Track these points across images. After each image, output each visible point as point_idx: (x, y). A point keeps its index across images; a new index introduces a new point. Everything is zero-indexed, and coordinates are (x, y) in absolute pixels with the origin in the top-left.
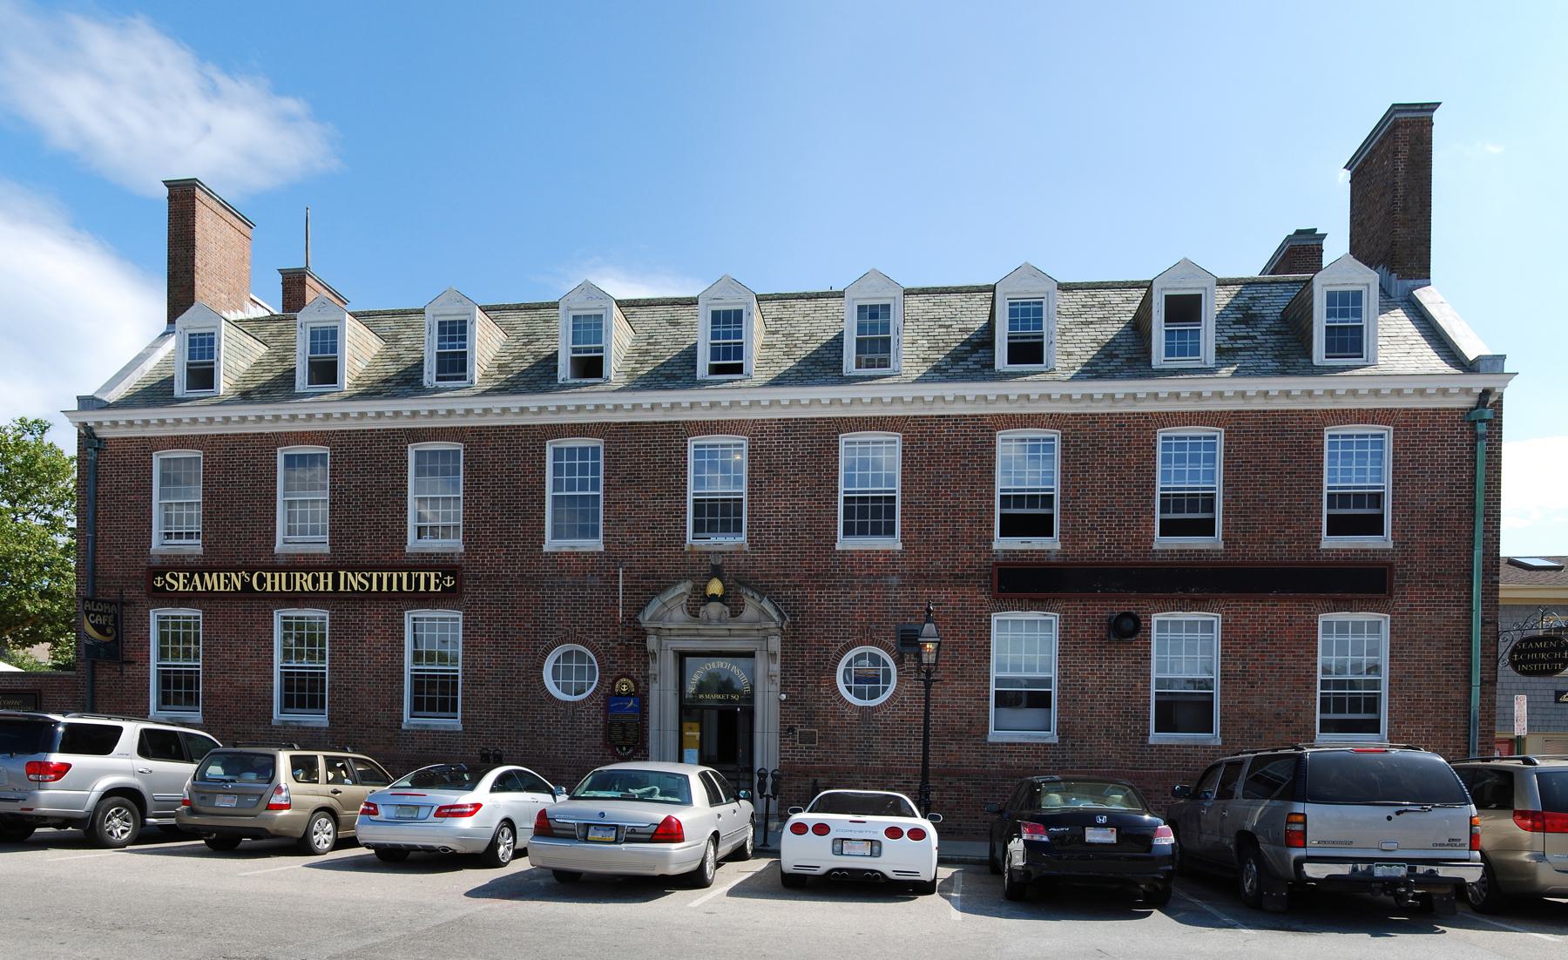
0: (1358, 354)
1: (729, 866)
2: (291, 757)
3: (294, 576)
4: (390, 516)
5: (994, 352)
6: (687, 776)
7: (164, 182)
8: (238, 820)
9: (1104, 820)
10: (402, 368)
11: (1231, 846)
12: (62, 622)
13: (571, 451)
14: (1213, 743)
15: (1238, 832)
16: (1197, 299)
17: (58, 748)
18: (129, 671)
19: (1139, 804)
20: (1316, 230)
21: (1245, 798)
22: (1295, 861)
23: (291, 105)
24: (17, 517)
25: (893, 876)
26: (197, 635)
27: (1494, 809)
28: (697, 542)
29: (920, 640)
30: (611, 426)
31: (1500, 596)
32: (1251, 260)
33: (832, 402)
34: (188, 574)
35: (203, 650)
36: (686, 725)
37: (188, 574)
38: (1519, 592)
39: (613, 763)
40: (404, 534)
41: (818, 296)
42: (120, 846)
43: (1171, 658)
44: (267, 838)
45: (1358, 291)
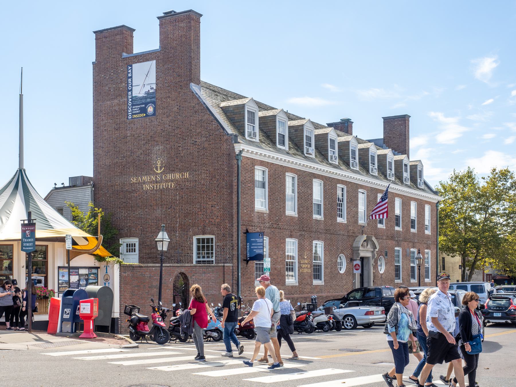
0: (46, 262)
1: (92, 258)
2: (109, 326)
3: (314, 263)
4: (200, 177)
5: (410, 175)
6: (420, 161)
7: (383, 118)
8: (439, 260)
9: (391, 181)
10: (472, 279)
11: (223, 330)
12: (507, 271)
13: (203, 240)
14: (400, 282)
15: (99, 261)
16: (388, 341)
17: (79, 328)
18: (39, 263)
19: (151, 329)
20: (351, 120)
21: (281, 315)
22: (467, 286)
23: (203, 313)
24: (500, 223)
25: (27, 280)
26: (212, 246)
27: (22, 229)
28: (400, 249)
29: (169, 240)
30: (331, 144)
31: (255, 207)
32: (147, 91)
33: (432, 199)
34: (153, 336)
35: (204, 234)
36: (45, 250)
37: (153, 336)
38: (95, 350)
39: (348, 373)
40: (140, 244)
41: (137, 86)
42: (262, 163)
43: (205, 253)
44: (235, 98)
45: (359, 150)
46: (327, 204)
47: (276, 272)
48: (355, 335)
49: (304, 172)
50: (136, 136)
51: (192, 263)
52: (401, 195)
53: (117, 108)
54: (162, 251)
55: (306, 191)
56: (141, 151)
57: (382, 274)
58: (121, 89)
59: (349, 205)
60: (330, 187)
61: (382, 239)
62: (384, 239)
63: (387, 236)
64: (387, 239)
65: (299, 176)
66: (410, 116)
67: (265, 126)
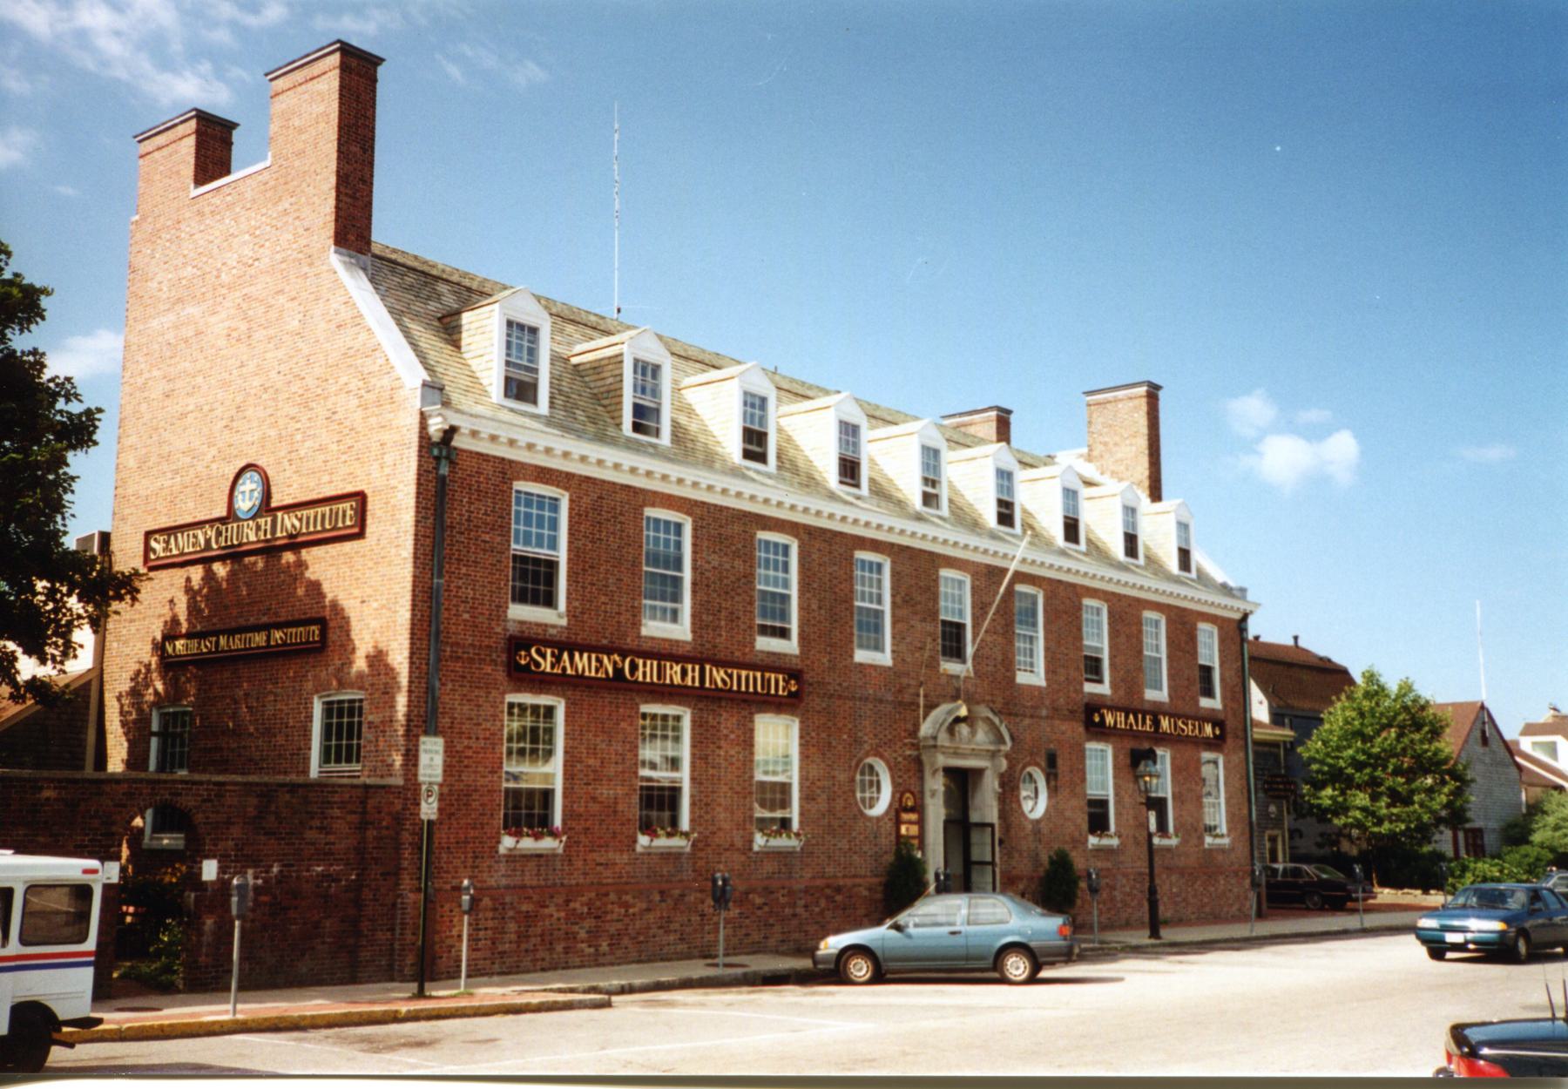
46: (814, 607)
47: (594, 807)
48: (1169, 972)
49: (721, 509)
50: (206, 408)
51: (146, 769)
52: (892, 545)
53: (170, 336)
54: (637, 763)
55: (727, 566)
56: (214, 451)
57: (1038, 822)
58: (184, 282)
59: (900, 613)
60: (826, 559)
61: (1032, 717)
62: (1041, 718)
63: (1055, 709)
64: (1052, 718)
65: (1221, 629)
66: (382, 60)
67: (596, 377)
